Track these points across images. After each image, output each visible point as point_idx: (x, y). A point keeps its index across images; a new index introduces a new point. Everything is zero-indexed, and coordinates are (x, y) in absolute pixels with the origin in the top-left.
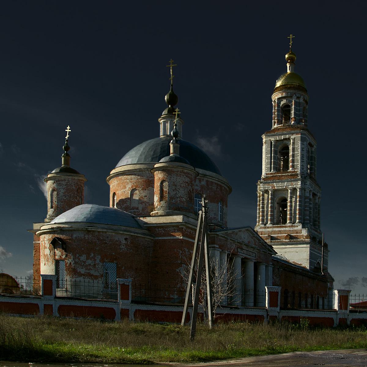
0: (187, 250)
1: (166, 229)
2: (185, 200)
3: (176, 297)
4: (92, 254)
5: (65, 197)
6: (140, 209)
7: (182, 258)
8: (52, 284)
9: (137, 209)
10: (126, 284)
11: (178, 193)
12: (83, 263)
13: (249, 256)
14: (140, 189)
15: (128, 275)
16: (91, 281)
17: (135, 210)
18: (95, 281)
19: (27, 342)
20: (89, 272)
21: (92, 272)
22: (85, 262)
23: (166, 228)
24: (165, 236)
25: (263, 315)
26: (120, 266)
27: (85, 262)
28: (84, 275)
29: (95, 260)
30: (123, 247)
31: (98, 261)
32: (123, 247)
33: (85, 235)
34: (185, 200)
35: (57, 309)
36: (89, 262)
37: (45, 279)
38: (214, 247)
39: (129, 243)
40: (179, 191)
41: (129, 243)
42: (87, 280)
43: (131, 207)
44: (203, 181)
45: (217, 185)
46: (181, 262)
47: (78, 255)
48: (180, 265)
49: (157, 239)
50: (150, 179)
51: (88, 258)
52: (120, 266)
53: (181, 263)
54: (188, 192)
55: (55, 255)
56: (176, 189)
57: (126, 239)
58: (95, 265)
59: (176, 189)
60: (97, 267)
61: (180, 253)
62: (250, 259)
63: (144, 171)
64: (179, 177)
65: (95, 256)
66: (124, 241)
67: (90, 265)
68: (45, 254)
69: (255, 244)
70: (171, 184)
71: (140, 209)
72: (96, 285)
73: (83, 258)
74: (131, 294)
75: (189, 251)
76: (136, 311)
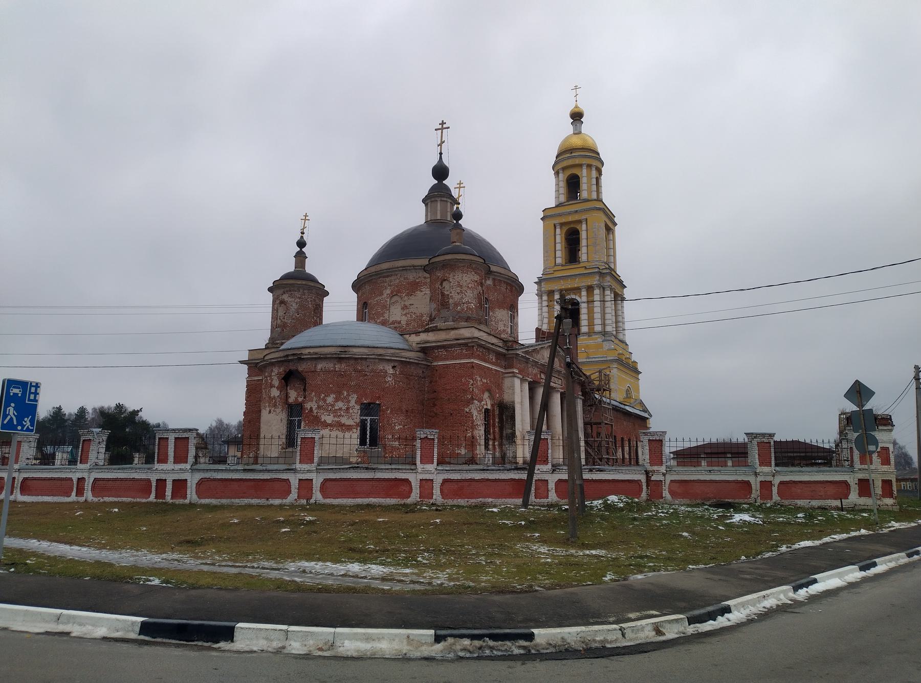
0: (479, 379)
1: (450, 349)
2: (474, 307)
3: (463, 451)
4: (345, 393)
5: (298, 314)
6: (403, 323)
7: (473, 390)
8: (434, 447)
9: (400, 322)
10: (430, 437)
11: (464, 296)
12: (330, 407)
13: (555, 384)
14: (404, 295)
15: (396, 421)
16: (340, 434)
17: (396, 325)
18: (347, 435)
19: (813, 591)
20: (339, 419)
21: (344, 420)
22: (333, 406)
23: (448, 348)
24: (447, 359)
25: (640, 479)
26: (384, 407)
27: (333, 406)
28: (330, 425)
29: (349, 402)
30: (389, 379)
31: (352, 403)
32: (389, 379)
33: (335, 364)
34: (474, 307)
35: (320, 486)
36: (340, 404)
37: (303, 436)
38: (513, 372)
39: (398, 373)
40: (466, 294)
41: (398, 373)
42: (334, 433)
43: (391, 321)
44: (489, 280)
45: (506, 284)
46: (472, 397)
47: (323, 395)
48: (470, 402)
49: (436, 364)
50: (417, 280)
51: (337, 400)
52: (384, 407)
53: (472, 399)
54: (478, 295)
55: (287, 397)
56: (461, 292)
57: (394, 367)
58: (348, 409)
59: (461, 292)
60: (351, 411)
61: (471, 383)
62: (555, 388)
63: (409, 269)
64: (466, 274)
65: (348, 395)
66: (392, 370)
67: (340, 409)
68: (272, 396)
69: (560, 366)
70: (454, 285)
71: (403, 323)
72: (347, 441)
73: (330, 399)
74: (663, 461)
75: (481, 380)
76: (445, 481)
